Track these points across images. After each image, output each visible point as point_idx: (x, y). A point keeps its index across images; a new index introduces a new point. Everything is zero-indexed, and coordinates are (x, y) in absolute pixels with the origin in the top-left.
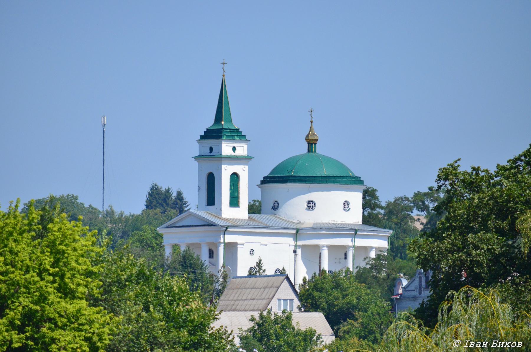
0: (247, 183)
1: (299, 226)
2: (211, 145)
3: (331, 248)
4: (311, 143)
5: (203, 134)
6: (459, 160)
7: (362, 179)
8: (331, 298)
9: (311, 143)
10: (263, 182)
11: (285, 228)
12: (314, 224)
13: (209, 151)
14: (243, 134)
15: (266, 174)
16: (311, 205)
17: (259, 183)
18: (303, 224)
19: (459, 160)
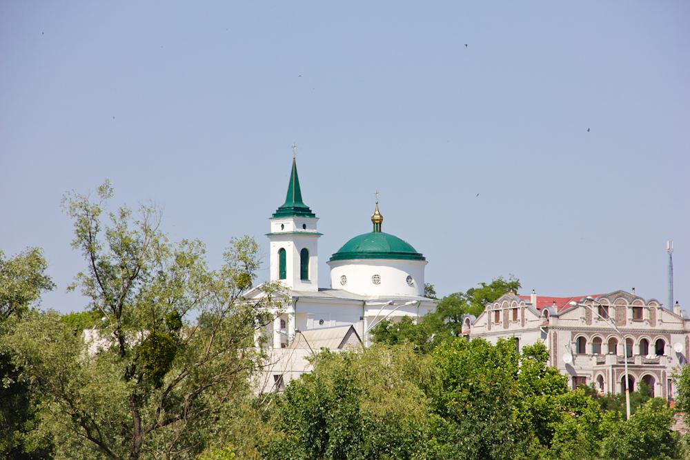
0: (400, 271)
1: (365, 299)
2: (282, 223)
3: (617, 370)
4: (378, 223)
5: (275, 212)
6: (111, 215)
7: (424, 256)
8: (510, 391)
9: (378, 223)
10: (332, 259)
11: (550, 344)
12: (380, 297)
13: (281, 228)
14: (313, 212)
15: (336, 251)
16: (376, 279)
17: (329, 260)
18: (369, 297)
19: (111, 215)
